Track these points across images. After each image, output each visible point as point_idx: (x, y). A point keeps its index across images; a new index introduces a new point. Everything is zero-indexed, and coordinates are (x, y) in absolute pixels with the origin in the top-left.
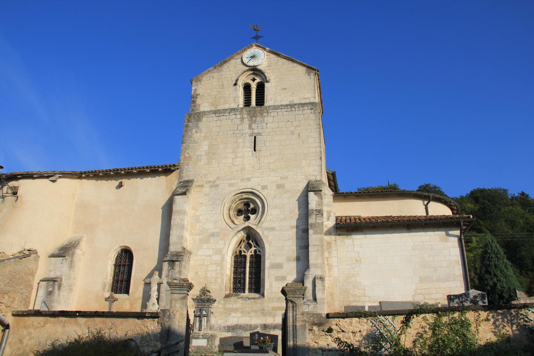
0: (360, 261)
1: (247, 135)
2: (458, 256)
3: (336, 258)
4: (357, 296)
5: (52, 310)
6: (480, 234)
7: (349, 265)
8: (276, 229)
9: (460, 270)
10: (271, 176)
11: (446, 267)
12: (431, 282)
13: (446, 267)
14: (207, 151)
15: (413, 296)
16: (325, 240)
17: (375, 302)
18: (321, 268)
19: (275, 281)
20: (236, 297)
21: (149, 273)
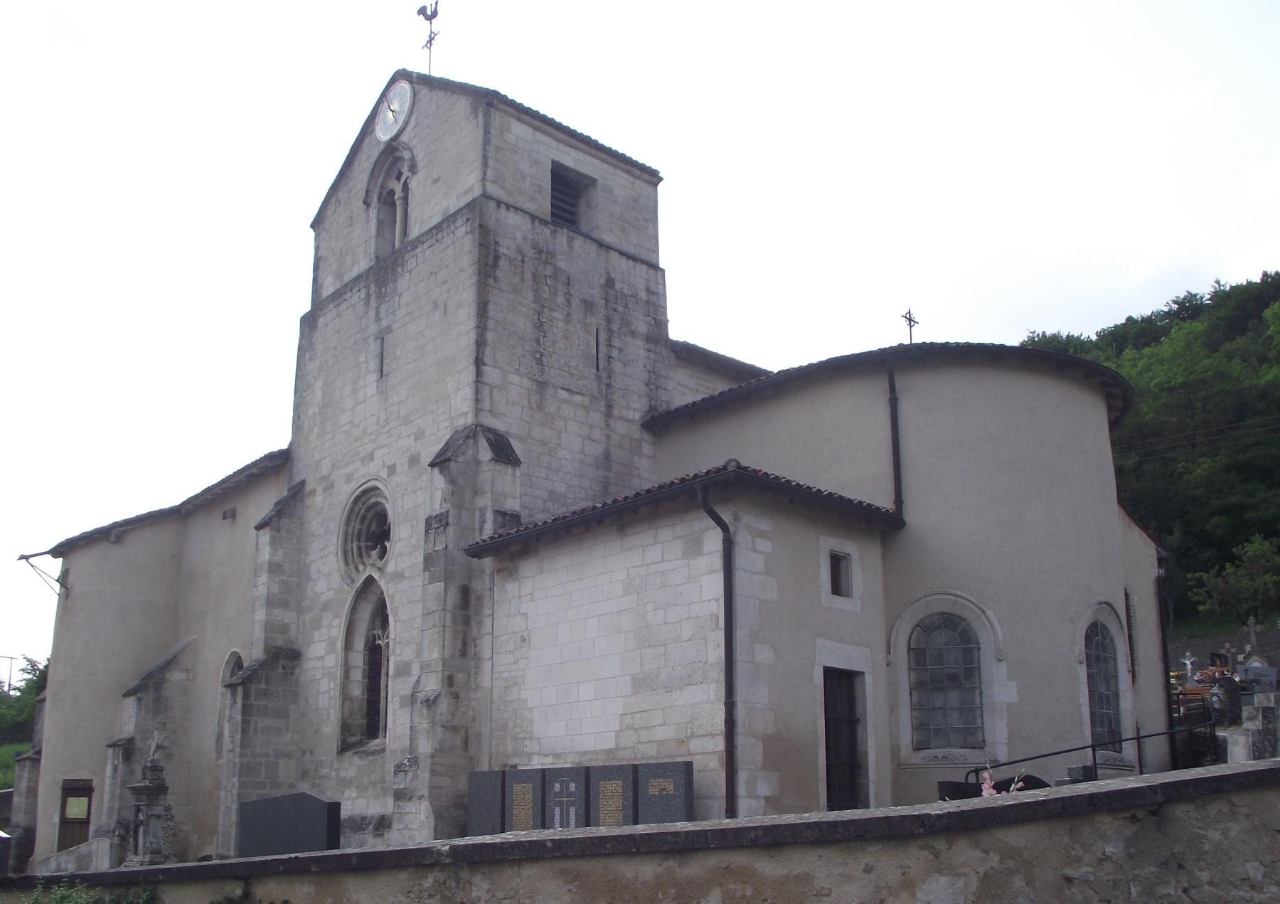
0: (529, 640)
1: (372, 339)
2: (717, 600)
3: (490, 636)
4: (520, 738)
5: (720, 514)
6: (1208, 359)
7: (510, 653)
8: (406, 574)
9: (718, 646)
10: (404, 438)
11: (690, 640)
12: (654, 690)
13: (690, 640)
14: (321, 403)
15: (617, 733)
16: (338, 588)
17: (546, 755)
18: (554, 596)
19: (400, 708)
20: (351, 752)
21: (847, 494)
